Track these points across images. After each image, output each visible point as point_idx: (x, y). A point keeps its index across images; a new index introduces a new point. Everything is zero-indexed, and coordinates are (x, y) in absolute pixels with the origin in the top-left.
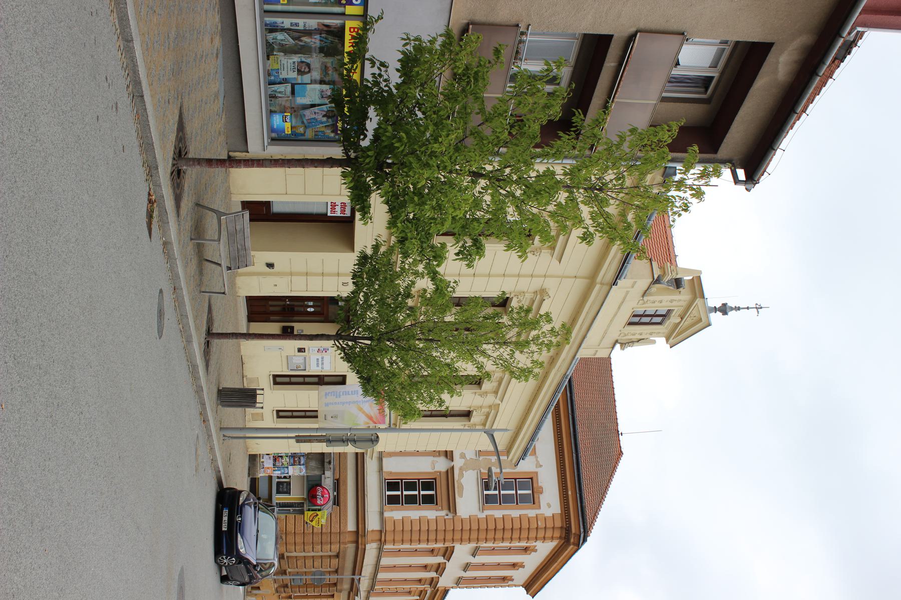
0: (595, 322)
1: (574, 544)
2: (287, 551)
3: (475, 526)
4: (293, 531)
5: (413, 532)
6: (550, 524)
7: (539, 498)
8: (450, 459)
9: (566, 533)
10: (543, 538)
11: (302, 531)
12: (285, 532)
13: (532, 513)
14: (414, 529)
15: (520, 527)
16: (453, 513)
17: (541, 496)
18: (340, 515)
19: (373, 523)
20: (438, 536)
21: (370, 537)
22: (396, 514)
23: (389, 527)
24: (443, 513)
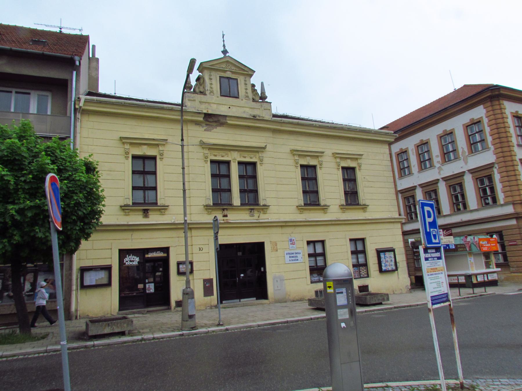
1: (499, 91)
3: (499, 150)
5: (510, 185)
8: (464, 173)
9: (494, 98)
10: (510, 152)
13: (485, 121)
14: (509, 190)
15: (503, 163)
17: (475, 118)
20: (506, 146)
22: (501, 197)
23: (510, 199)
24: (495, 171)
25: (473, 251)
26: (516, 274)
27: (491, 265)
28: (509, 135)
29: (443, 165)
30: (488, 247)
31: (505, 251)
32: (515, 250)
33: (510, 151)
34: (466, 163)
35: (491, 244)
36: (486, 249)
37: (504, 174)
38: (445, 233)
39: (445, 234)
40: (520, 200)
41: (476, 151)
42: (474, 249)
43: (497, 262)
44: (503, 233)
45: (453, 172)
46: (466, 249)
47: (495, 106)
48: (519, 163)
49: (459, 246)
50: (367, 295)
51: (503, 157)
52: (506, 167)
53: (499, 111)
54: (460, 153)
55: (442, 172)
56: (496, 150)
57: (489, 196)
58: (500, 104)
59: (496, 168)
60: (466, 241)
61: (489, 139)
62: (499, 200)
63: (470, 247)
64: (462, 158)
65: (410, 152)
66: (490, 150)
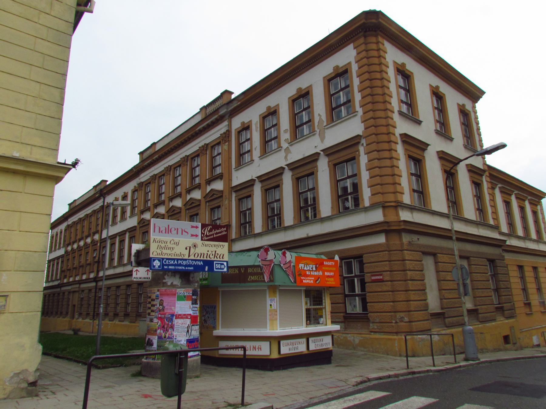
0: (350, 158)
2: (426, 310)
4: (392, 304)
6: (363, 47)
7: (342, 67)
8: (319, 156)
11: (390, 293)
12: (393, 314)
13: (355, 68)
16: (360, 139)
18: (370, 253)
19: (377, 216)
21: (392, 218)
23: (379, 198)
24: (362, 149)
25: (276, 284)
26: (377, 336)
27: (321, 317)
28: (399, 189)
29: (291, 145)
30: (317, 278)
31: (365, 291)
32: (380, 290)
33: (390, 150)
34: (322, 139)
35: (324, 272)
36: (312, 282)
37: (375, 155)
38: (206, 232)
39: (207, 236)
40: (395, 202)
41: (339, 117)
42: (280, 278)
43: (353, 310)
44: (364, 259)
45: (304, 155)
46: (264, 278)
47: (371, 44)
48: (399, 141)
49: (250, 270)
50: (459, 294)
51: (374, 119)
52: (378, 151)
53: (375, 53)
54: (316, 124)
55: (289, 157)
56: (365, 114)
57: (351, 194)
58: (378, 43)
59: (363, 144)
60: (265, 260)
61: (358, 97)
62: (363, 200)
63: (272, 273)
64: (318, 131)
65: (254, 127)
66: (356, 115)
